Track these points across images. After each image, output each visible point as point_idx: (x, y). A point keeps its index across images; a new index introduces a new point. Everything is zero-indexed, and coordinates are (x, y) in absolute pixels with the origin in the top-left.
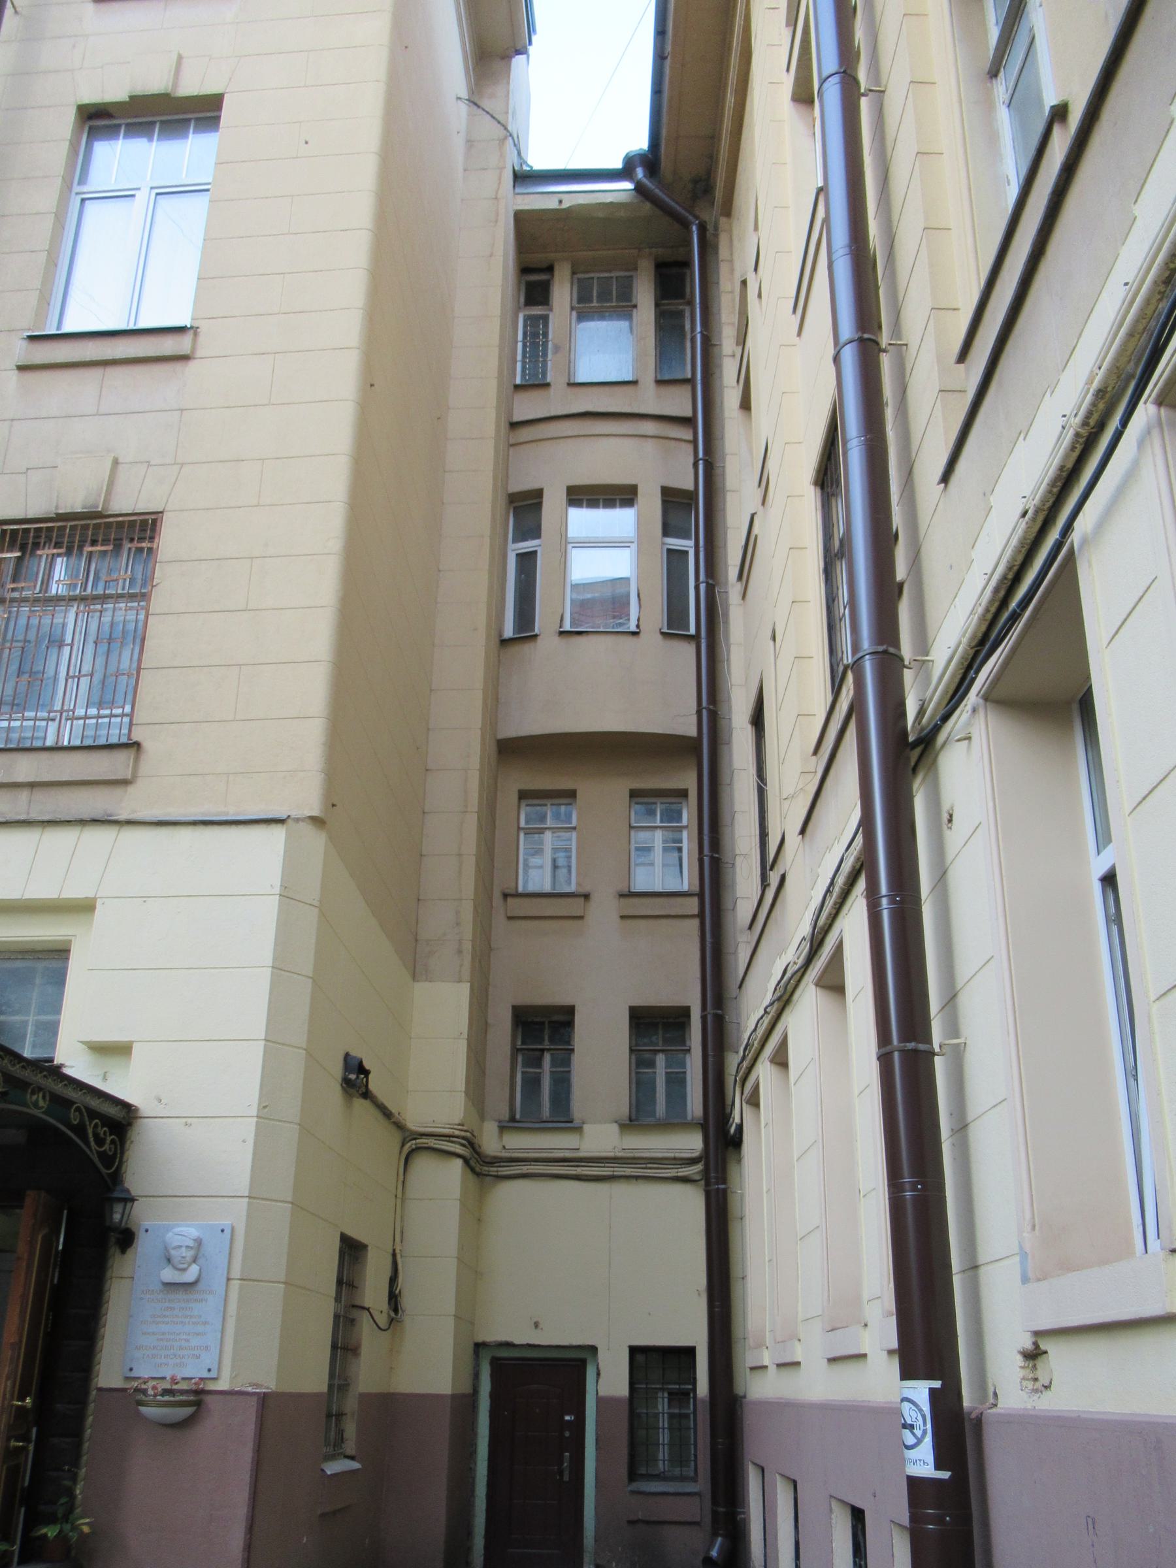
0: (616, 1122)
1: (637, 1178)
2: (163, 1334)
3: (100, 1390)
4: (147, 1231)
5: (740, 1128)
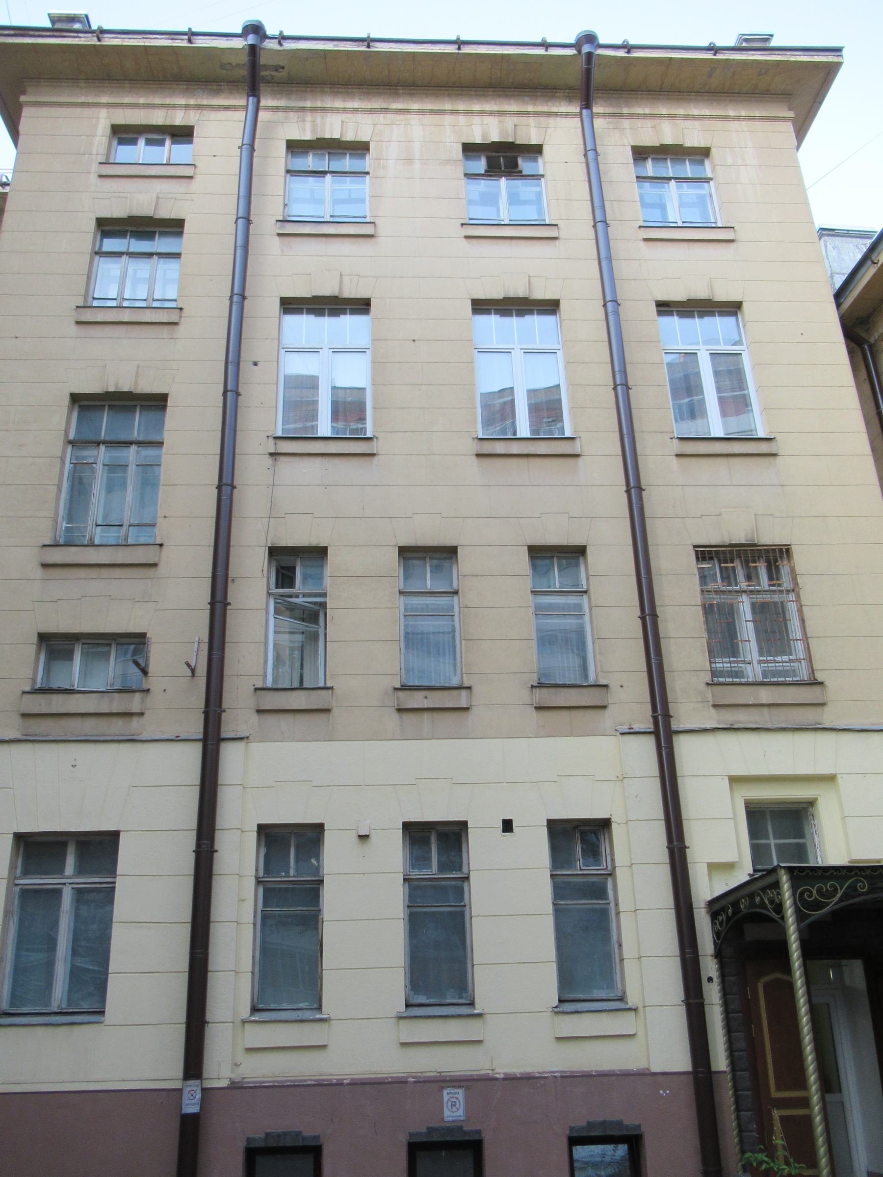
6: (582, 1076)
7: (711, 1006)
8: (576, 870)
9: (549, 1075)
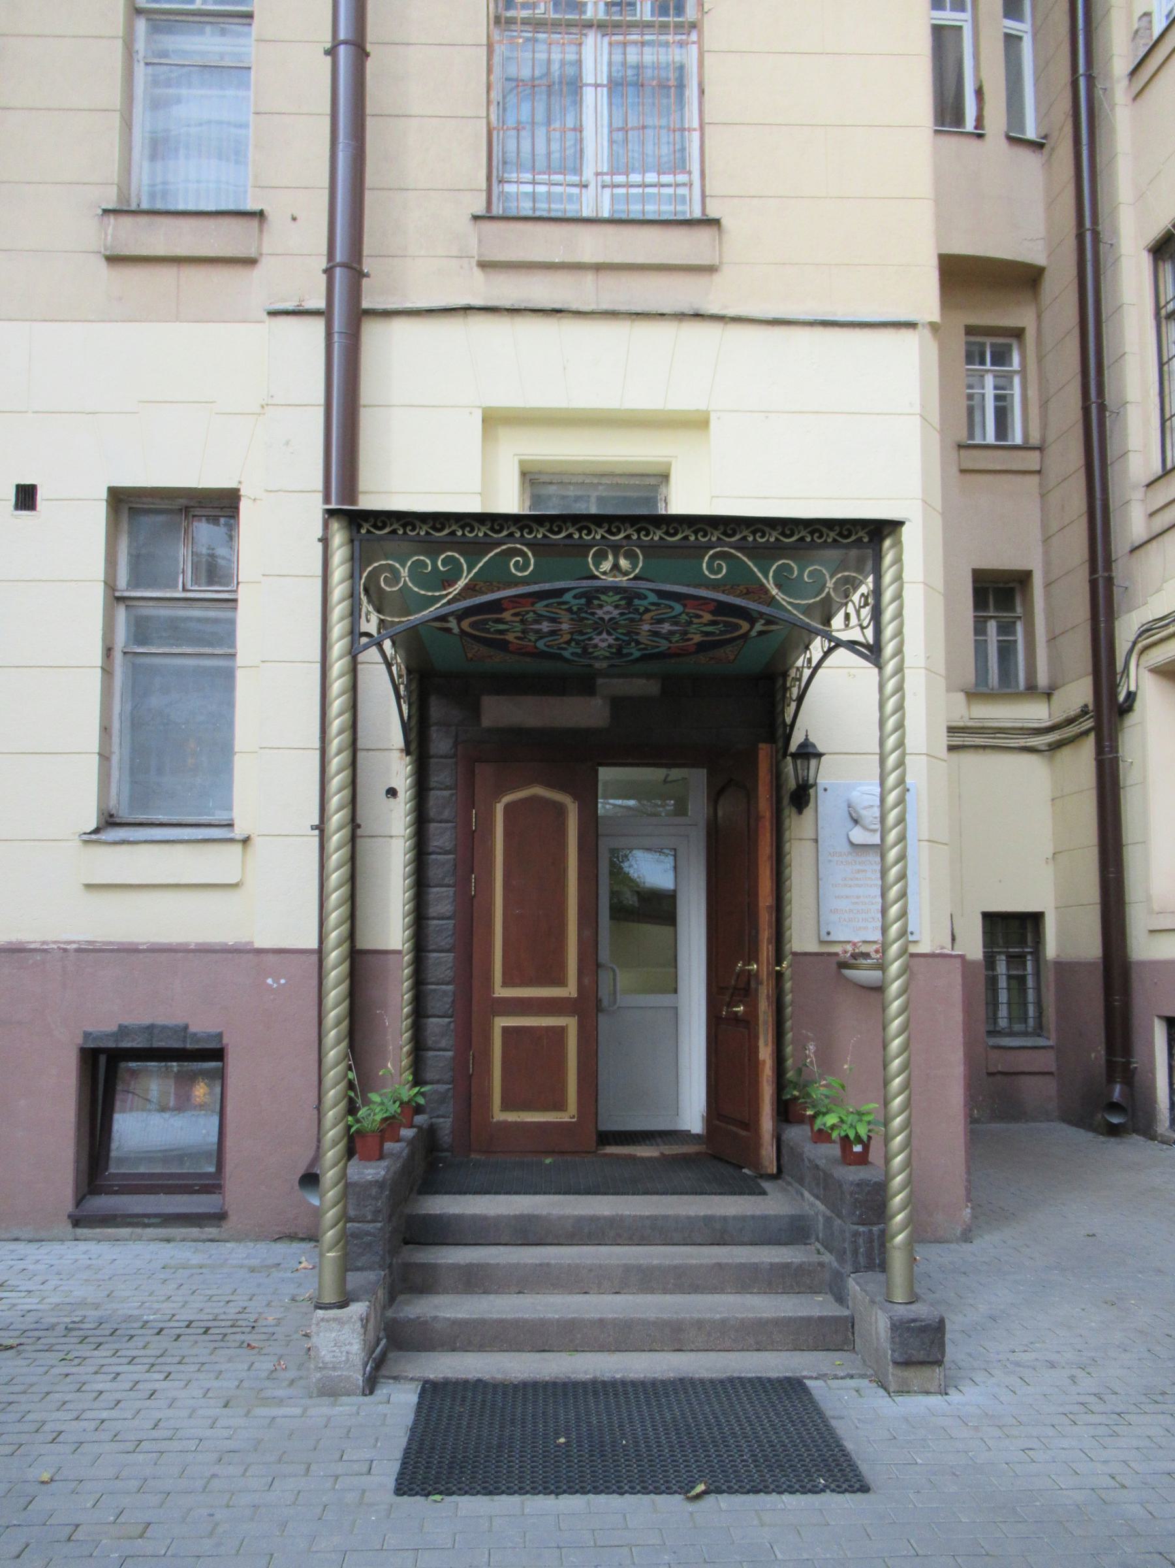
0: (962, 691)
1: (984, 747)
2: (858, 897)
3: (795, 954)
4: (825, 790)
5: (1131, 696)
6: (118, 950)
7: (388, 839)
8: (178, 591)
9: (55, 946)
